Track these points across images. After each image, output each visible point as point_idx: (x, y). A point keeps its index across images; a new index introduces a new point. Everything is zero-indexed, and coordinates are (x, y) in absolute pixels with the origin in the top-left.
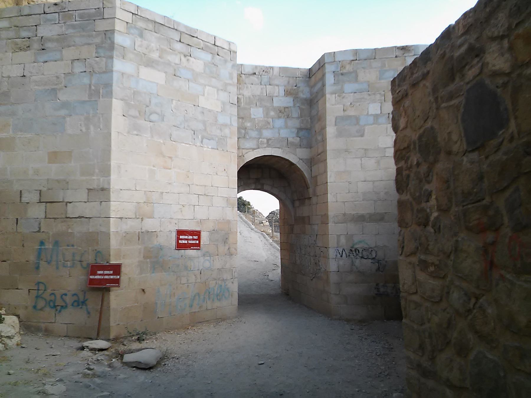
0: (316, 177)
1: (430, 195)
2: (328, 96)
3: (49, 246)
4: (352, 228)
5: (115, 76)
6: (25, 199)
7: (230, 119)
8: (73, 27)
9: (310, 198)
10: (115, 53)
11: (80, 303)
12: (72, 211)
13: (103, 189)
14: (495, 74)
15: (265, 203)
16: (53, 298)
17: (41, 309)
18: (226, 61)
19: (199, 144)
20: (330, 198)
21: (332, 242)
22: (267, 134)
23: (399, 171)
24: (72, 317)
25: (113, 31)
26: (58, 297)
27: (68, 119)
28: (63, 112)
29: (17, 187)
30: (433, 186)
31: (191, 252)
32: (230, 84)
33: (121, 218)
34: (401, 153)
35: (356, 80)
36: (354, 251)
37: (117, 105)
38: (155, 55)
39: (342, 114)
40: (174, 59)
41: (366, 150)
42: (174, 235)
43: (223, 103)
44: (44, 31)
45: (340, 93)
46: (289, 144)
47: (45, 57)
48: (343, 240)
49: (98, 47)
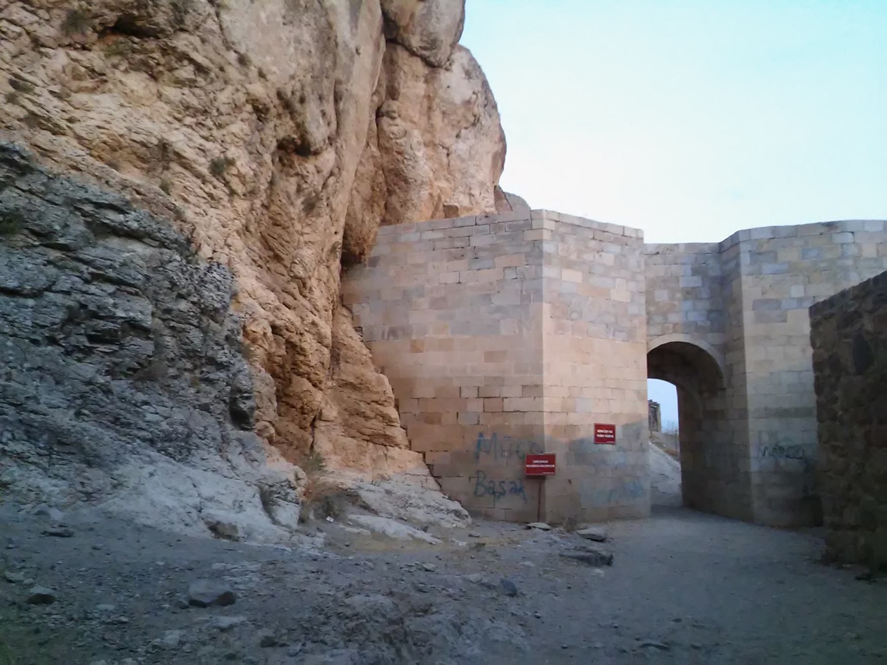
0: (731, 365)
1: (837, 398)
2: (744, 278)
3: (488, 437)
4: (776, 424)
5: (544, 281)
6: (464, 395)
7: (639, 309)
8: (503, 237)
9: (724, 389)
10: (544, 261)
11: (517, 491)
12: (508, 406)
13: (537, 386)
14: (868, 333)
15: (665, 394)
16: (491, 485)
17: (481, 496)
18: (634, 250)
19: (611, 337)
20: (750, 390)
21: (753, 439)
22: (674, 318)
23: (817, 378)
24: (511, 503)
25: (541, 241)
26: (497, 484)
27: (502, 322)
28: (497, 316)
29: (456, 384)
30: (838, 393)
31: (608, 447)
32: (638, 273)
33: (551, 412)
34: (818, 365)
35: (775, 259)
36: (778, 450)
37: (546, 307)
38: (573, 257)
39: (759, 297)
40: (588, 257)
41: (789, 337)
42: (592, 429)
43: (632, 293)
44: (476, 241)
45: (757, 274)
46: (698, 328)
47: (477, 266)
48: (765, 438)
49: (528, 255)
